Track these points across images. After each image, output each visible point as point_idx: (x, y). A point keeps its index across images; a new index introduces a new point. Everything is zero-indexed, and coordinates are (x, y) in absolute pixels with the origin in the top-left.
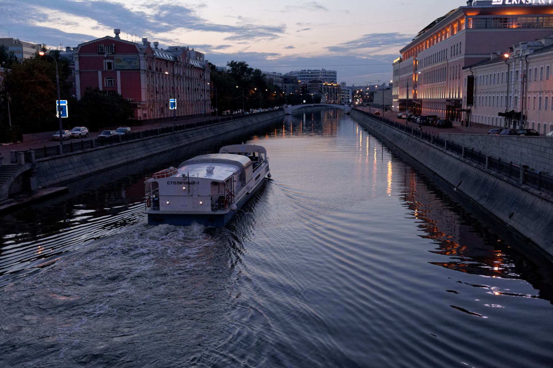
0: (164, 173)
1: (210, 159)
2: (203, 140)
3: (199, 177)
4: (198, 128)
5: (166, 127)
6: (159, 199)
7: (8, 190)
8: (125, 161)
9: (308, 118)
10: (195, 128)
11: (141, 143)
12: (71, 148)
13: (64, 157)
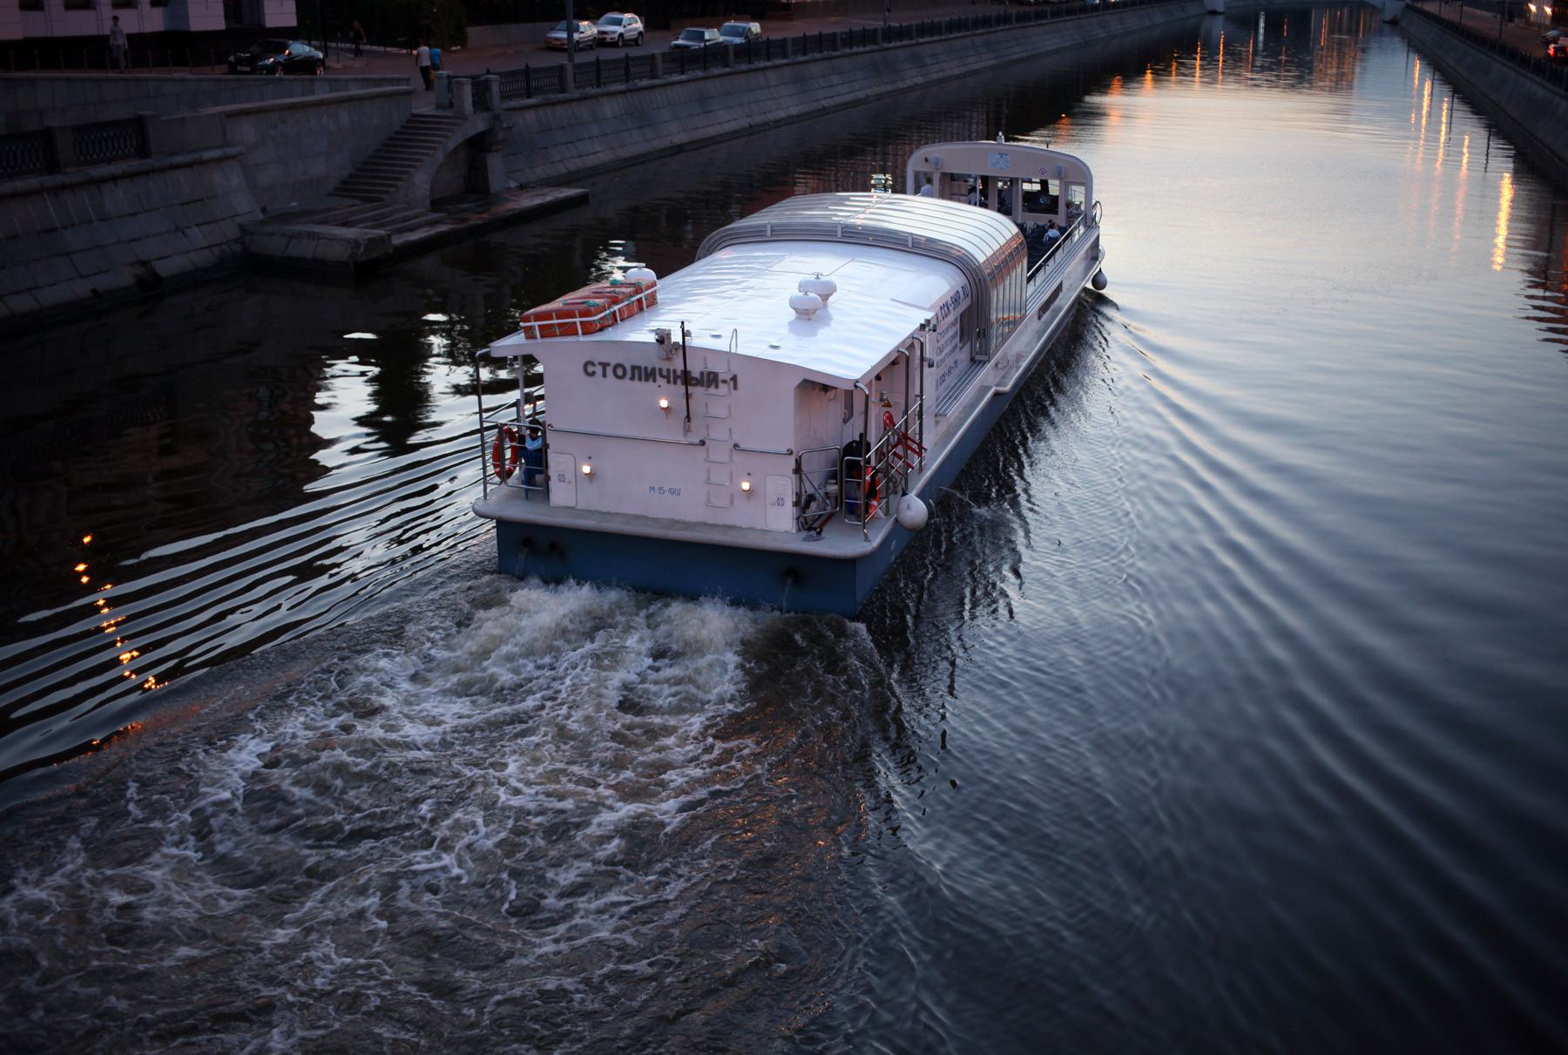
0: (571, 314)
1: (835, 225)
2: (964, 75)
3: (740, 351)
4: (952, 36)
5: (861, 28)
6: (546, 446)
7: (428, 186)
8: (744, 123)
9: (1273, 28)
10: (943, 37)
11: (787, 72)
12: (597, 74)
13: (579, 99)
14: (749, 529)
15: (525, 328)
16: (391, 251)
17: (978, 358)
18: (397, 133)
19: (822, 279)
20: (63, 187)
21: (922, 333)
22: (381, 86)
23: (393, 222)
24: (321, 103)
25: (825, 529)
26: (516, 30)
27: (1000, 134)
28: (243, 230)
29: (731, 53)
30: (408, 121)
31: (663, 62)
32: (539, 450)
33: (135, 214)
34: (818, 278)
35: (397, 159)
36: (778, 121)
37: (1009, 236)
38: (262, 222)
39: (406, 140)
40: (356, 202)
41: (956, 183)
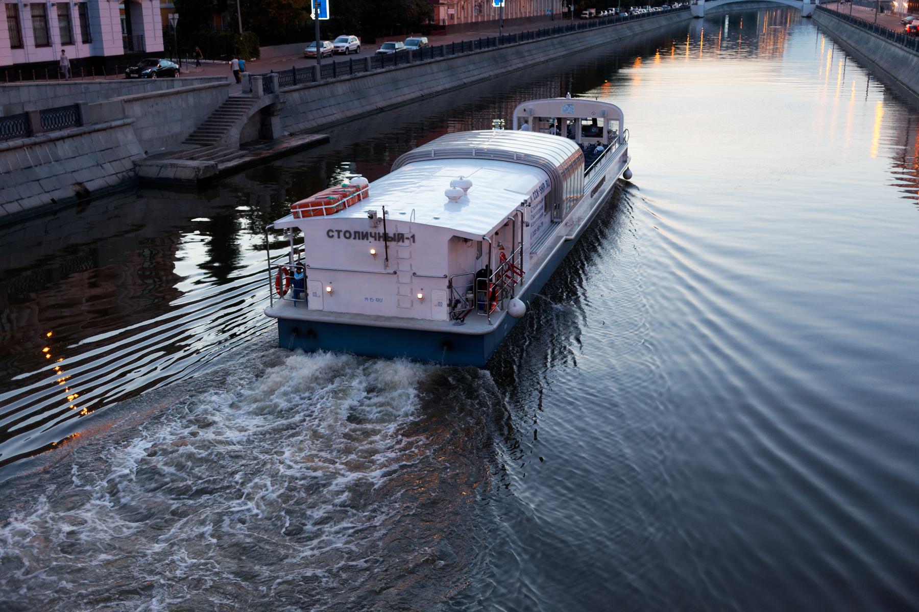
7: (238, 136)
8: (418, 94)
11: (443, 64)
17: (555, 220)
18: (220, 107)
20: (35, 144)
23: (219, 157)
28: (134, 163)
30: (227, 101)
36: (438, 92)
37: (573, 151)
38: (145, 159)
40: (198, 146)
41: (542, 122)
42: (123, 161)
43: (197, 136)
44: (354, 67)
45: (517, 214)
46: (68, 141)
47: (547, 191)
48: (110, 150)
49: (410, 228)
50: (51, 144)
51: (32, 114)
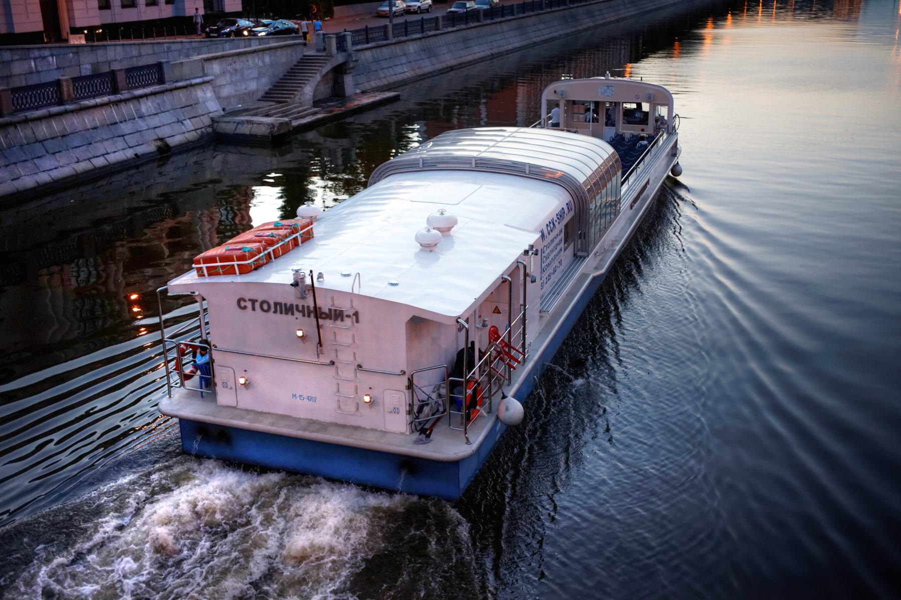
7: (311, 94)
8: (488, 53)
11: (514, 23)
14: (372, 430)
15: (197, 268)
16: (291, 129)
17: (580, 254)
18: (295, 65)
19: (447, 214)
20: (121, 101)
21: (526, 257)
22: (286, 41)
23: (293, 113)
24: (254, 52)
25: (435, 430)
26: (360, 7)
27: (608, 72)
28: (212, 120)
29: (482, 15)
30: (301, 59)
31: (443, 21)
32: (208, 363)
33: (157, 114)
34: (442, 214)
35: (295, 80)
36: (508, 51)
37: (606, 156)
38: (223, 116)
39: (300, 69)
40: (273, 103)
41: (576, 106)
42: (202, 117)
43: (272, 94)
44: (425, 26)
45: (518, 267)
46: (151, 98)
47: (567, 219)
48: (190, 108)
49: (352, 301)
50: (135, 102)
51: (118, 73)
